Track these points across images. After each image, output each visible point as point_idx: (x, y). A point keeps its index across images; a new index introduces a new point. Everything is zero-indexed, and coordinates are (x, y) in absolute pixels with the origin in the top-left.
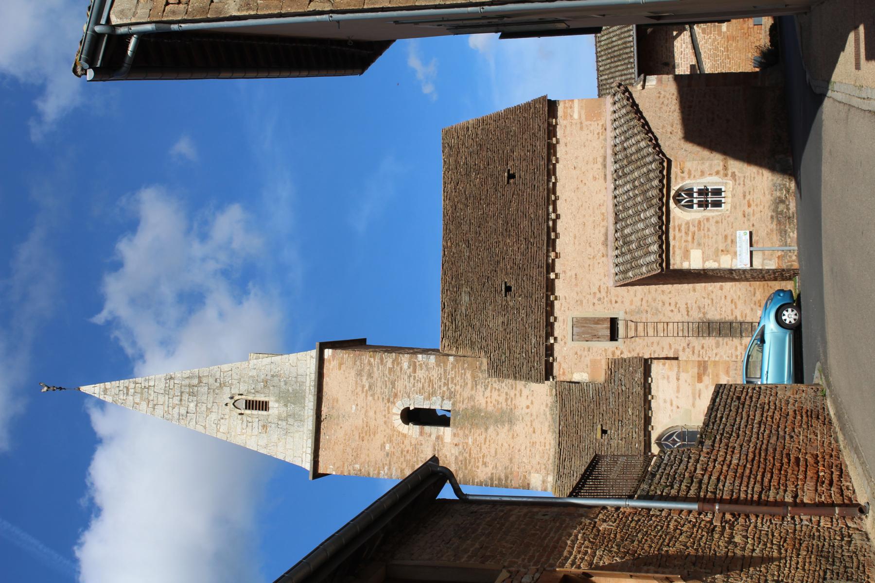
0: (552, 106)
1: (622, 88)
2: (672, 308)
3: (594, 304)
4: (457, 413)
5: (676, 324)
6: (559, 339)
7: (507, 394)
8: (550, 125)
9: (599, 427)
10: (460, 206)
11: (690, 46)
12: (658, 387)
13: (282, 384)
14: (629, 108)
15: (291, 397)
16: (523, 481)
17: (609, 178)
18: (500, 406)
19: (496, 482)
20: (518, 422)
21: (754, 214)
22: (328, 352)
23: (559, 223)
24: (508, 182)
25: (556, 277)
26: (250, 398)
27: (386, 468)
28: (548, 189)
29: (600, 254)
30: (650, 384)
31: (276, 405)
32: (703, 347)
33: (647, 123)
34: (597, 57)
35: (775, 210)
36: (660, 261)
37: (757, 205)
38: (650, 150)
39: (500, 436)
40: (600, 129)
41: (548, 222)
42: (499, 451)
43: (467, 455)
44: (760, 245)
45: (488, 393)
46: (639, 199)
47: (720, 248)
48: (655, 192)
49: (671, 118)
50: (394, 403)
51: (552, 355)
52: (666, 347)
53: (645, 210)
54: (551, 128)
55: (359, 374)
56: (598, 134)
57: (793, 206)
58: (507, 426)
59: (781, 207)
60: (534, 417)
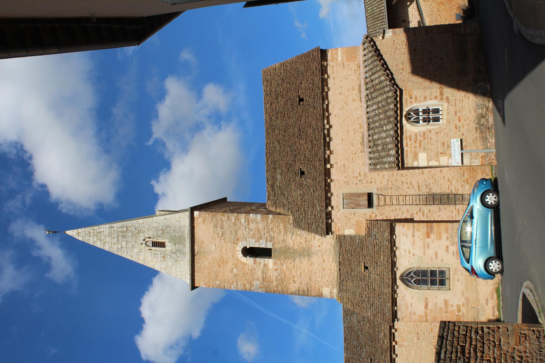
0: (323, 54)
1: (369, 39)
2: (409, 185)
3: (356, 184)
4: (276, 250)
5: (411, 197)
6: (335, 207)
7: (306, 238)
8: (322, 66)
9: (363, 264)
10: (274, 118)
11: (417, 10)
12: (400, 241)
13: (172, 232)
14: (373, 53)
15: (178, 240)
16: (318, 292)
17: (364, 99)
18: (302, 246)
19: (301, 293)
20: (313, 256)
21: (463, 127)
22: (196, 213)
23: (332, 132)
24: (299, 104)
25: (331, 167)
26: (154, 240)
27: (235, 284)
28: (323, 109)
29: (359, 151)
30: (394, 240)
31: (170, 244)
32: (430, 211)
33: (385, 63)
34: (367, 19)
35: (479, 123)
36: (397, 162)
37: (465, 120)
38: (388, 83)
39: (303, 264)
40: (355, 67)
41: (324, 131)
42: (303, 273)
43: (283, 276)
44: (469, 149)
45: (294, 237)
46: (382, 116)
47: (440, 151)
48: (391, 113)
49: (402, 58)
50: (237, 244)
51: (330, 218)
52: (405, 211)
53: (386, 125)
54: (324, 68)
55: (216, 226)
56: (355, 70)
57: (491, 120)
58: (307, 258)
59: (483, 121)
60: (324, 252)
